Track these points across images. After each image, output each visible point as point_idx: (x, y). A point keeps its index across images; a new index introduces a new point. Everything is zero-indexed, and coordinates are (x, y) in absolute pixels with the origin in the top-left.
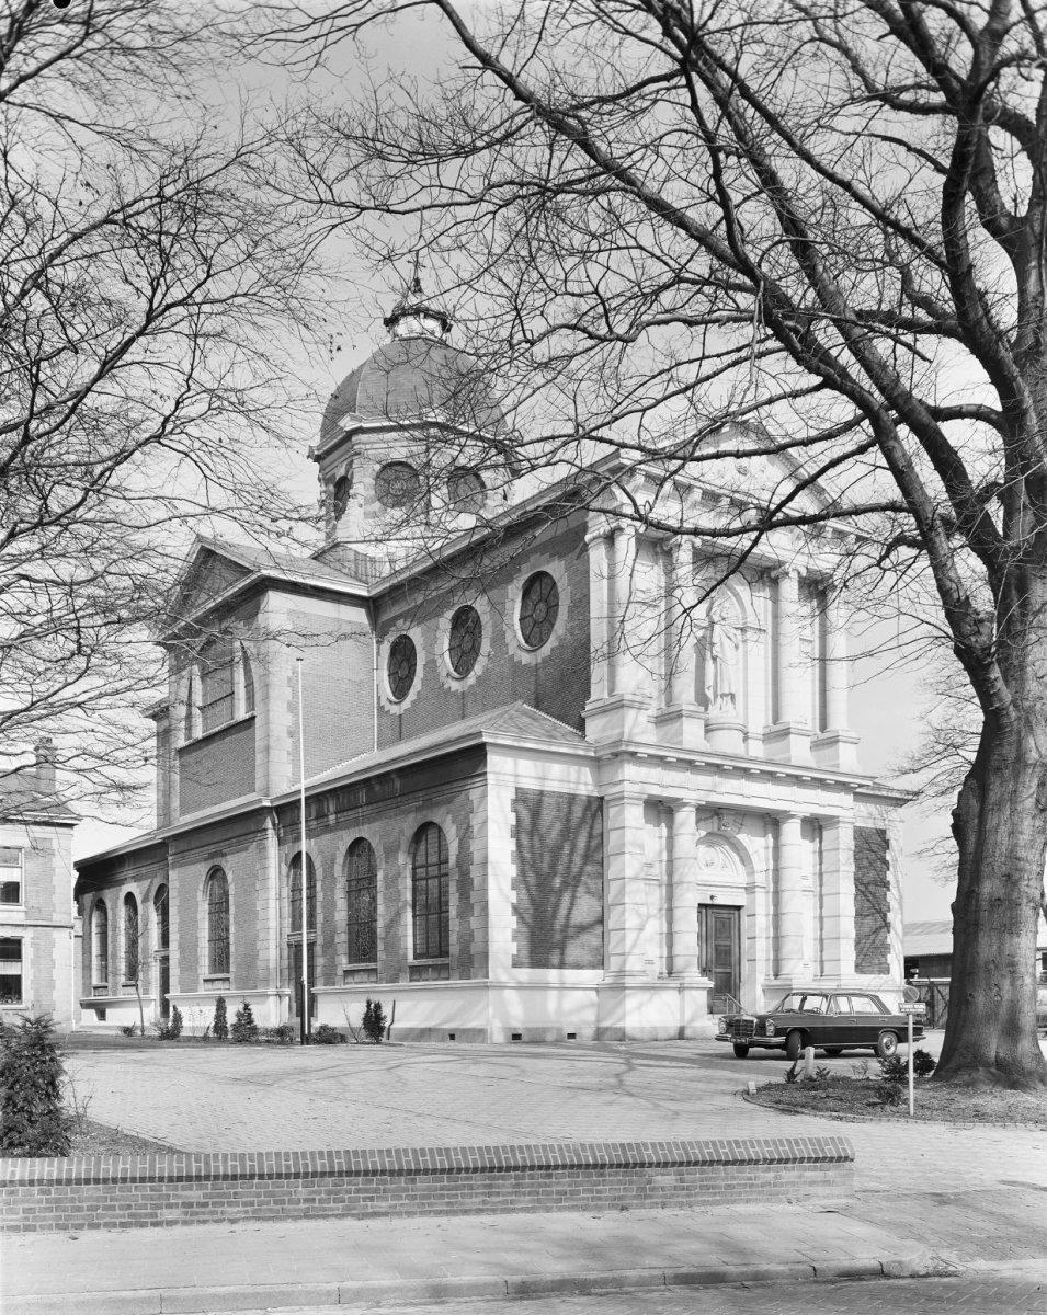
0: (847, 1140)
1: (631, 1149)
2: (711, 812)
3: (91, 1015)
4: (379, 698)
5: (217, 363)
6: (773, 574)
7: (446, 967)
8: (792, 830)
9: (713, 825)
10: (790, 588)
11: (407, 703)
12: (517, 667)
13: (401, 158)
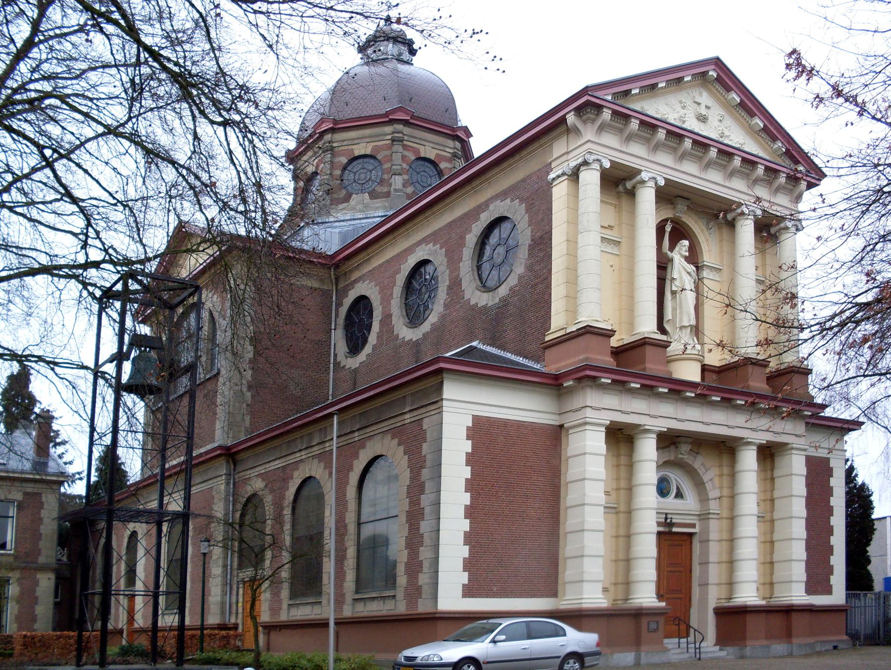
0: (111, 247)
2: (668, 440)
3: (813, 449)
4: (335, 355)
6: (730, 217)
8: (749, 459)
10: (746, 230)
11: (362, 357)
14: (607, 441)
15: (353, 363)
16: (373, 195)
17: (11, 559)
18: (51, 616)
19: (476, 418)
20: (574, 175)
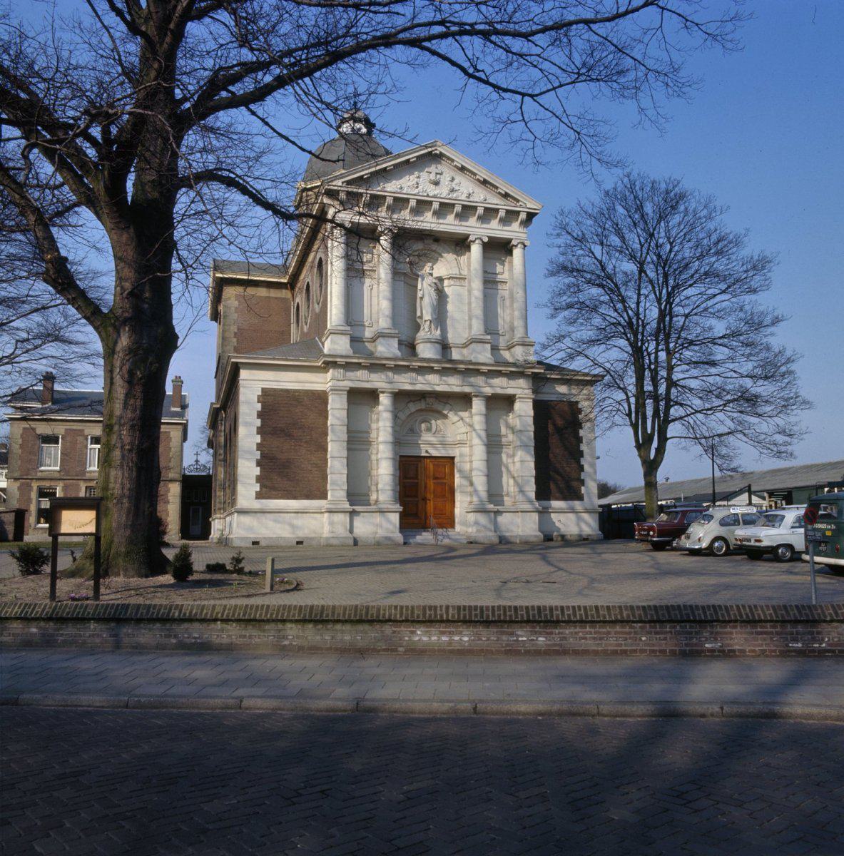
1: (557, 609)
2: (401, 397)
19: (263, 389)
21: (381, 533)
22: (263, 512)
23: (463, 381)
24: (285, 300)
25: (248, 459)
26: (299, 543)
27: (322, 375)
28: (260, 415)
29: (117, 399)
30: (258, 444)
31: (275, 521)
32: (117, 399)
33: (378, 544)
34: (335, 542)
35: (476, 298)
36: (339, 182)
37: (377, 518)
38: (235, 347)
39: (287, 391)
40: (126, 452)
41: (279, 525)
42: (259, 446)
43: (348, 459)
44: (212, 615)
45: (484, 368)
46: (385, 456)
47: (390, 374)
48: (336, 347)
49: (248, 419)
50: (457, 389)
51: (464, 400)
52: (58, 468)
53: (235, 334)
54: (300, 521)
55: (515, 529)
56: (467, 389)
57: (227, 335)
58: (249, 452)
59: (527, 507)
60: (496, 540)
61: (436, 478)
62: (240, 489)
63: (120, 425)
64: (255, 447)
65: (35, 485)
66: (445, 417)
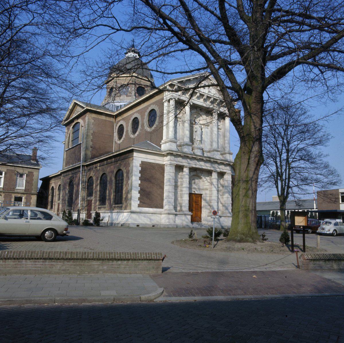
1: (80, 254)
2: (192, 170)
5: (108, 60)
7: (105, 208)
9: (195, 173)
11: (121, 141)
12: (147, 132)
13: (151, 17)
14: (175, 169)
15: (119, 142)
16: (127, 96)
17: (23, 191)
18: (15, 233)
19: (142, 162)
20: (169, 101)
21: (185, 223)
22: (140, 213)
23: (211, 165)
24: (112, 123)
25: (135, 190)
26: (153, 226)
27: (162, 158)
28: (140, 172)
29: (251, 170)
30: (139, 184)
31: (145, 217)
32: (251, 170)
33: (184, 228)
34: (170, 226)
35: (215, 134)
36: (176, 82)
37: (183, 217)
38: (92, 140)
39: (150, 163)
40: (253, 192)
41: (145, 219)
42: (140, 185)
43: (174, 192)
44: (7, 256)
45: (219, 161)
46: (186, 192)
47: (189, 160)
48: (172, 147)
49: (136, 173)
50: (209, 168)
51: (209, 173)
52: (24, 188)
53: (92, 134)
54: (154, 217)
55: (225, 223)
56: (212, 169)
57: (89, 134)
58: (136, 187)
59: (229, 215)
60: (220, 227)
61: (196, 202)
62: (133, 203)
63: (252, 181)
64: (138, 185)
65: (13, 195)
66: (201, 178)
